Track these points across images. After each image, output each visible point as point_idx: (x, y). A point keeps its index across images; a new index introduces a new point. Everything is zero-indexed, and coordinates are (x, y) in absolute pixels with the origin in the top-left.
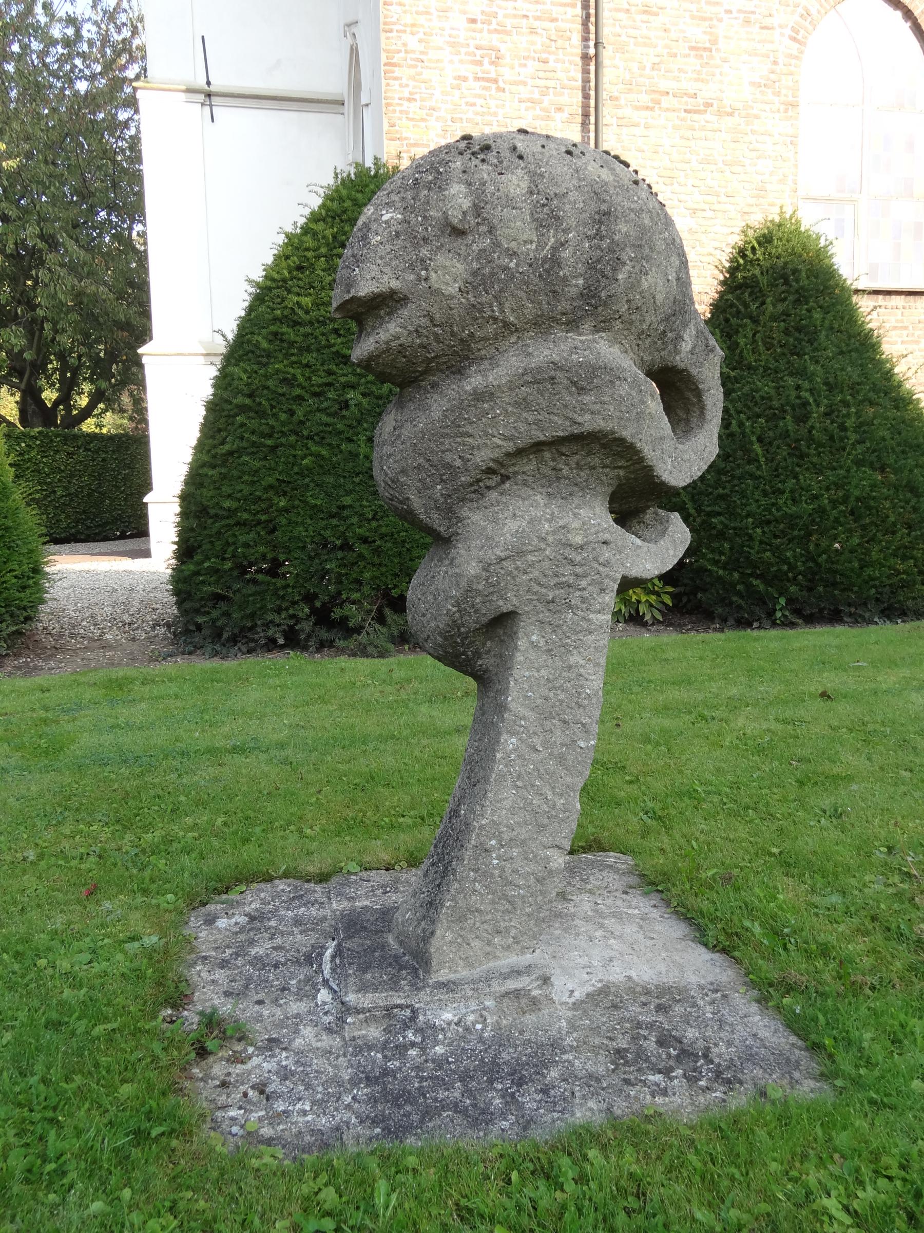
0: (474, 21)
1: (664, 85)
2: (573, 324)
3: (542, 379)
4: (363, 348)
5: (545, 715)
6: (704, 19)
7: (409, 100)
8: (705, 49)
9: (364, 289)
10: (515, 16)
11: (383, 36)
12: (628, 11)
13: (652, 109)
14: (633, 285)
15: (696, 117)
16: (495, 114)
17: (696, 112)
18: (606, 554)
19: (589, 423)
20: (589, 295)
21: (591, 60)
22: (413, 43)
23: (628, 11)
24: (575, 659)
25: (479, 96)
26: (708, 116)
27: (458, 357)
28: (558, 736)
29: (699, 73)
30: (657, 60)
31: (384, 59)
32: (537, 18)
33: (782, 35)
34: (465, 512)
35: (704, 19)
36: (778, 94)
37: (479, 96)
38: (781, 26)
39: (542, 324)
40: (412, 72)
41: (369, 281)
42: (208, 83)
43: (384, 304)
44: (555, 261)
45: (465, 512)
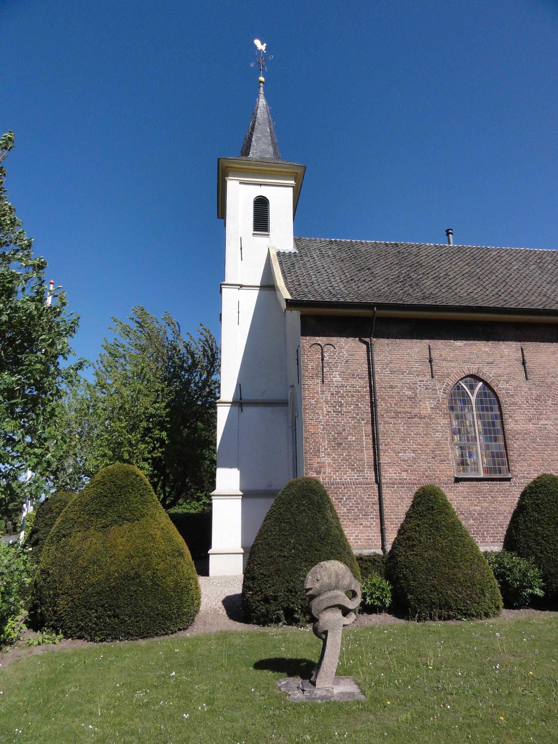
0: (333, 394)
1: (399, 410)
2: (334, 590)
3: (330, 598)
4: (308, 594)
5: (332, 646)
6: (412, 389)
7: (312, 420)
8: (413, 398)
9: (307, 587)
10: (346, 392)
11: (303, 400)
12: (385, 388)
13: (396, 418)
14: (342, 583)
15: (411, 420)
16: (341, 422)
17: (411, 418)
18: (340, 621)
19: (336, 603)
20: (336, 586)
21: (373, 405)
22: (313, 402)
23: (385, 388)
24: (336, 637)
25: (335, 417)
26: (416, 419)
27: (319, 595)
28: (334, 649)
29: (411, 405)
30: (396, 402)
31: (303, 407)
32: (353, 392)
33: (440, 392)
34: (320, 615)
35: (412, 389)
36: (441, 411)
37: (335, 417)
38: (439, 389)
39: (330, 590)
40: (313, 411)
41: (308, 586)
42: (241, 399)
43: (311, 589)
44: (331, 583)
45: (320, 615)
